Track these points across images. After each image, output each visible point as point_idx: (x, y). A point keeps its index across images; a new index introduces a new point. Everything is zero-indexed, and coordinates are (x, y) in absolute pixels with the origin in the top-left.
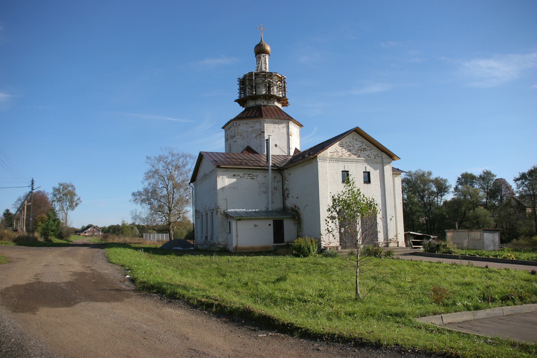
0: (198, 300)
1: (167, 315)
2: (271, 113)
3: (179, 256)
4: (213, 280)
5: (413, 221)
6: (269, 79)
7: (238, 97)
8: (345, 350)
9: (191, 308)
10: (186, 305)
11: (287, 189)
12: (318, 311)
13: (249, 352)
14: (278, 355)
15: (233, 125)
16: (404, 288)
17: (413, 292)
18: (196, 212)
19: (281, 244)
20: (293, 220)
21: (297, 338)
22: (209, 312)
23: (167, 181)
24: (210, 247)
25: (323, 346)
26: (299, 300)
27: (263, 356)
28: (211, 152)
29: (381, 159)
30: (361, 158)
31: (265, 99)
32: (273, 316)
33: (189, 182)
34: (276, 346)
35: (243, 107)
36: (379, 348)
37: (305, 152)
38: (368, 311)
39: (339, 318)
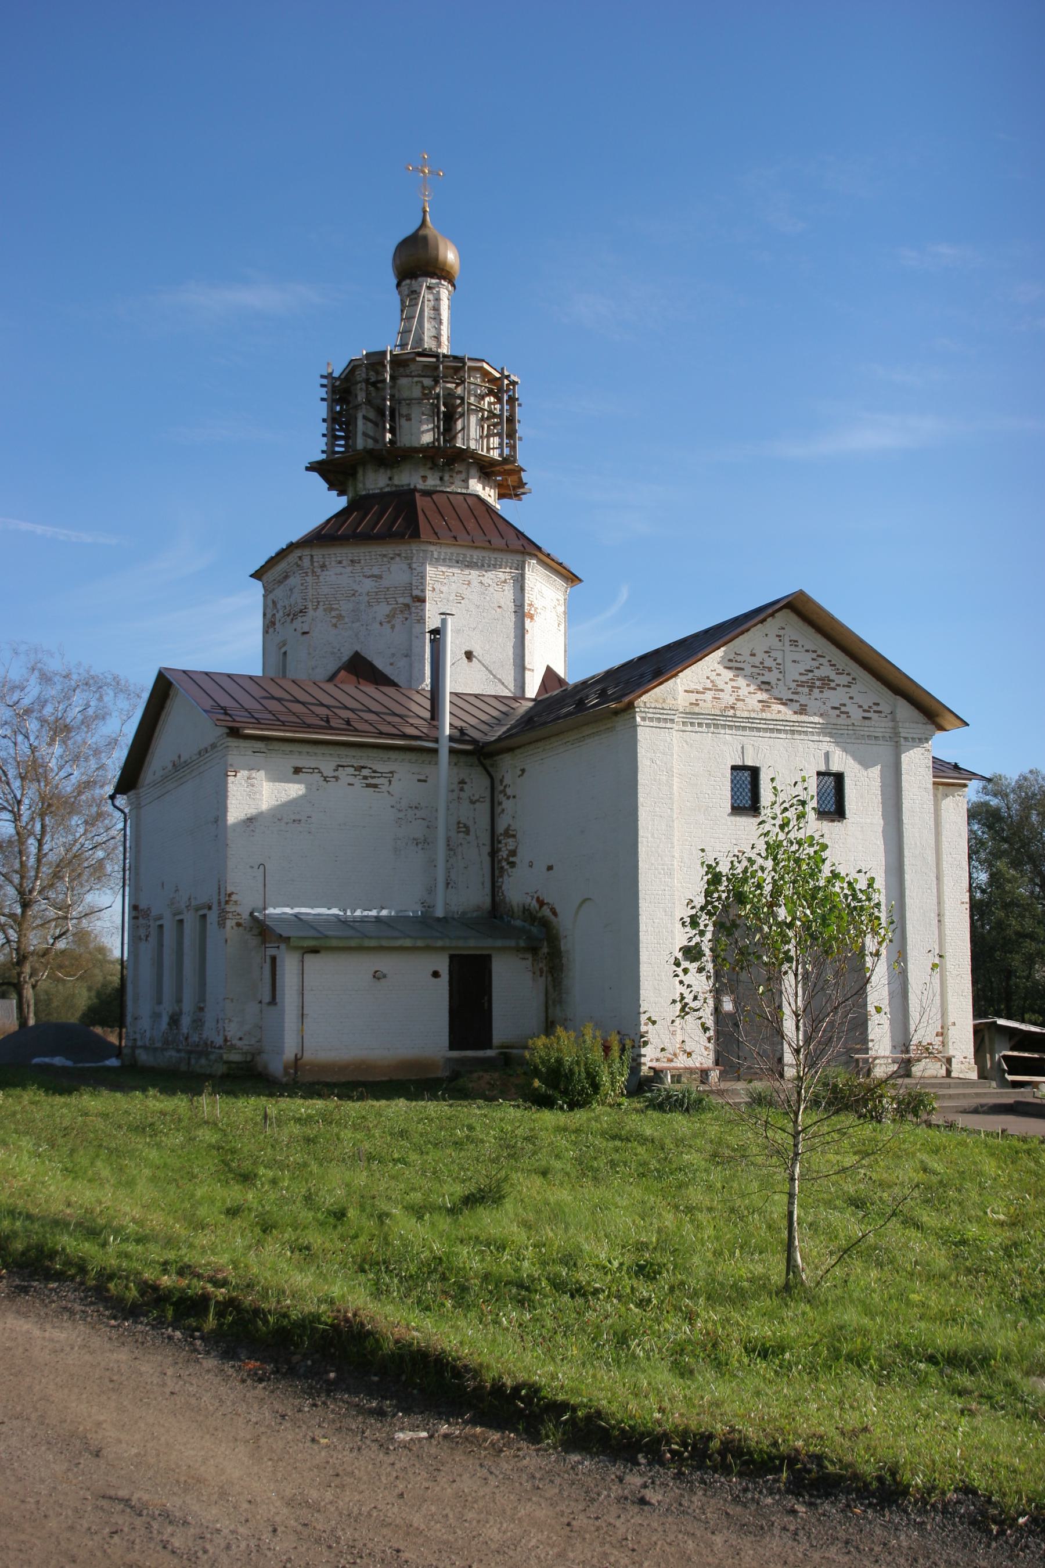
0: (145, 1282)
1: (10, 1349)
2: (454, 523)
3: (60, 1094)
4: (202, 1198)
5: (1009, 973)
6: (449, 385)
7: (323, 452)
8: (753, 1507)
9: (115, 1318)
10: (92, 1303)
11: (511, 832)
12: (636, 1335)
13: (356, 1511)
14: (479, 1522)
15: (298, 566)
16: (979, 1250)
17: (1016, 1268)
18: (137, 913)
19: (480, 1054)
20: (529, 956)
21: (555, 1448)
22: (190, 1332)
23: (16, 784)
24: (189, 1058)
25: (662, 1484)
26: (558, 1285)
27: (416, 1525)
28: (207, 674)
29: (891, 724)
30: (811, 719)
31: (429, 465)
32: (457, 1351)
33: (109, 790)
34: (467, 1484)
35: (338, 495)
36: (896, 1502)
37: (584, 684)
38: (839, 1341)
39: (720, 1365)
